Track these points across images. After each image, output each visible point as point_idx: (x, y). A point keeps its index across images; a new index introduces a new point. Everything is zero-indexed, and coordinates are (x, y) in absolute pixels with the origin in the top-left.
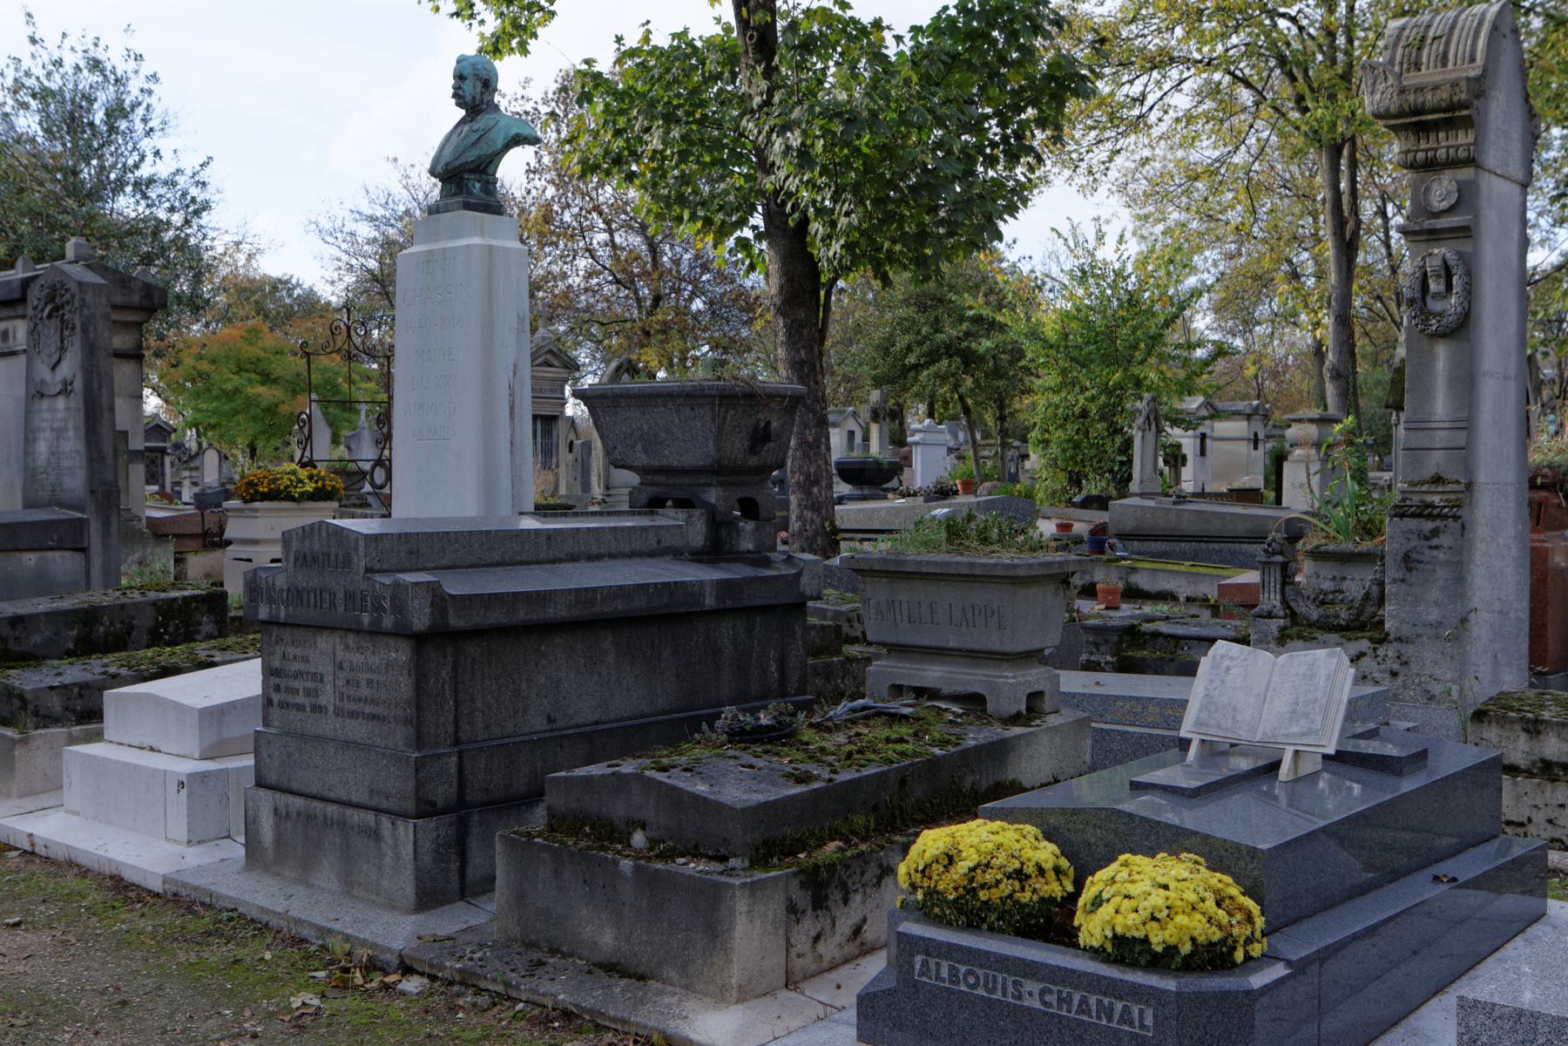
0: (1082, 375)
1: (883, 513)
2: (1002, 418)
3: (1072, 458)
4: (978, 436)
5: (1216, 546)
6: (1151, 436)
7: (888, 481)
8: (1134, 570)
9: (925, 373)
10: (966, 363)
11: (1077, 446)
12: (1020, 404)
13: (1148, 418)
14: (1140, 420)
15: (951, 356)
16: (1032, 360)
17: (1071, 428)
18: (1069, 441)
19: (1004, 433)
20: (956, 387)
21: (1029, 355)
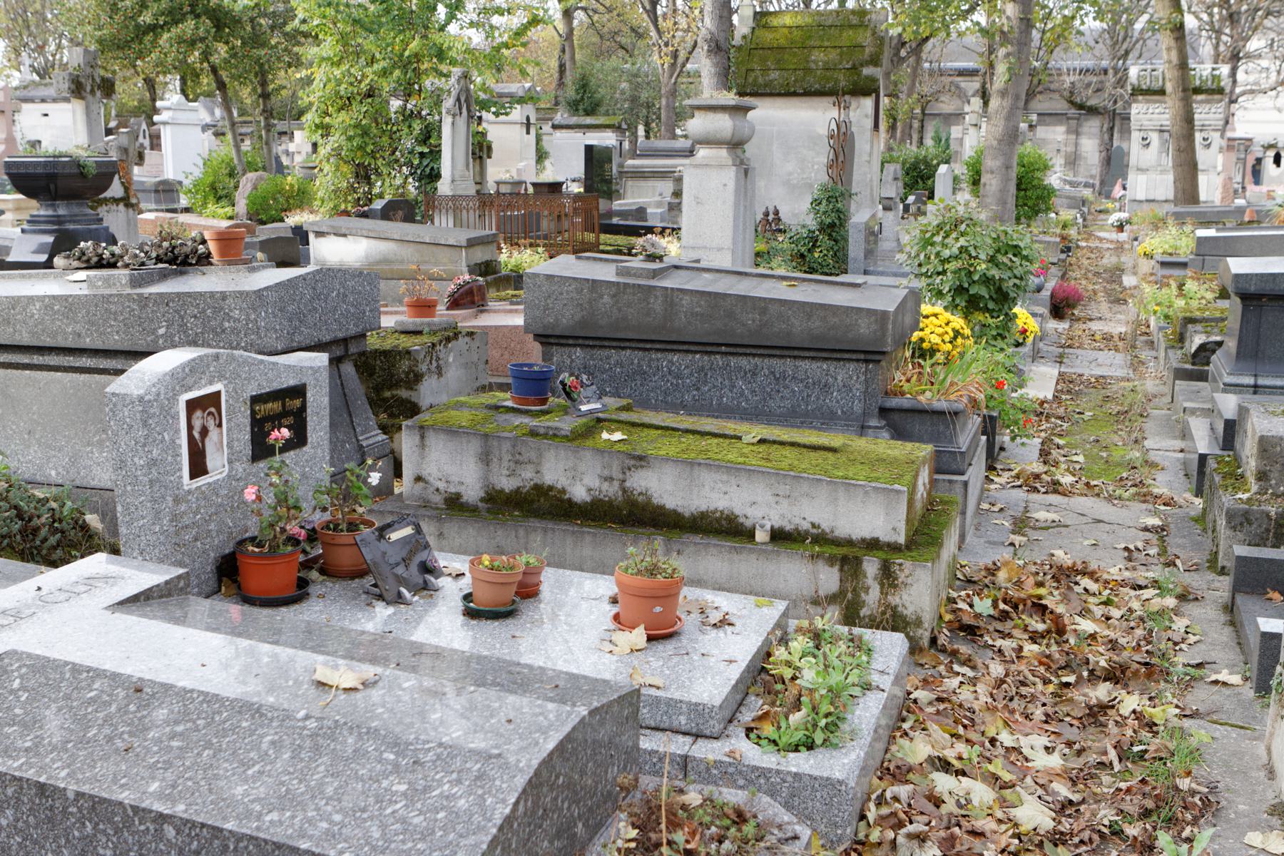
0: (368, 43)
1: (35, 309)
2: (265, 96)
3: (360, 148)
4: (235, 113)
5: (743, 362)
6: (462, 121)
7: (106, 188)
8: (641, 460)
9: (166, 36)
10: (219, 26)
11: (365, 133)
12: (283, 78)
13: (458, 100)
14: (449, 103)
15: (198, 16)
16: (304, 21)
17: (360, 110)
18: (355, 127)
19: (268, 113)
20: (206, 56)
21: (301, 15)
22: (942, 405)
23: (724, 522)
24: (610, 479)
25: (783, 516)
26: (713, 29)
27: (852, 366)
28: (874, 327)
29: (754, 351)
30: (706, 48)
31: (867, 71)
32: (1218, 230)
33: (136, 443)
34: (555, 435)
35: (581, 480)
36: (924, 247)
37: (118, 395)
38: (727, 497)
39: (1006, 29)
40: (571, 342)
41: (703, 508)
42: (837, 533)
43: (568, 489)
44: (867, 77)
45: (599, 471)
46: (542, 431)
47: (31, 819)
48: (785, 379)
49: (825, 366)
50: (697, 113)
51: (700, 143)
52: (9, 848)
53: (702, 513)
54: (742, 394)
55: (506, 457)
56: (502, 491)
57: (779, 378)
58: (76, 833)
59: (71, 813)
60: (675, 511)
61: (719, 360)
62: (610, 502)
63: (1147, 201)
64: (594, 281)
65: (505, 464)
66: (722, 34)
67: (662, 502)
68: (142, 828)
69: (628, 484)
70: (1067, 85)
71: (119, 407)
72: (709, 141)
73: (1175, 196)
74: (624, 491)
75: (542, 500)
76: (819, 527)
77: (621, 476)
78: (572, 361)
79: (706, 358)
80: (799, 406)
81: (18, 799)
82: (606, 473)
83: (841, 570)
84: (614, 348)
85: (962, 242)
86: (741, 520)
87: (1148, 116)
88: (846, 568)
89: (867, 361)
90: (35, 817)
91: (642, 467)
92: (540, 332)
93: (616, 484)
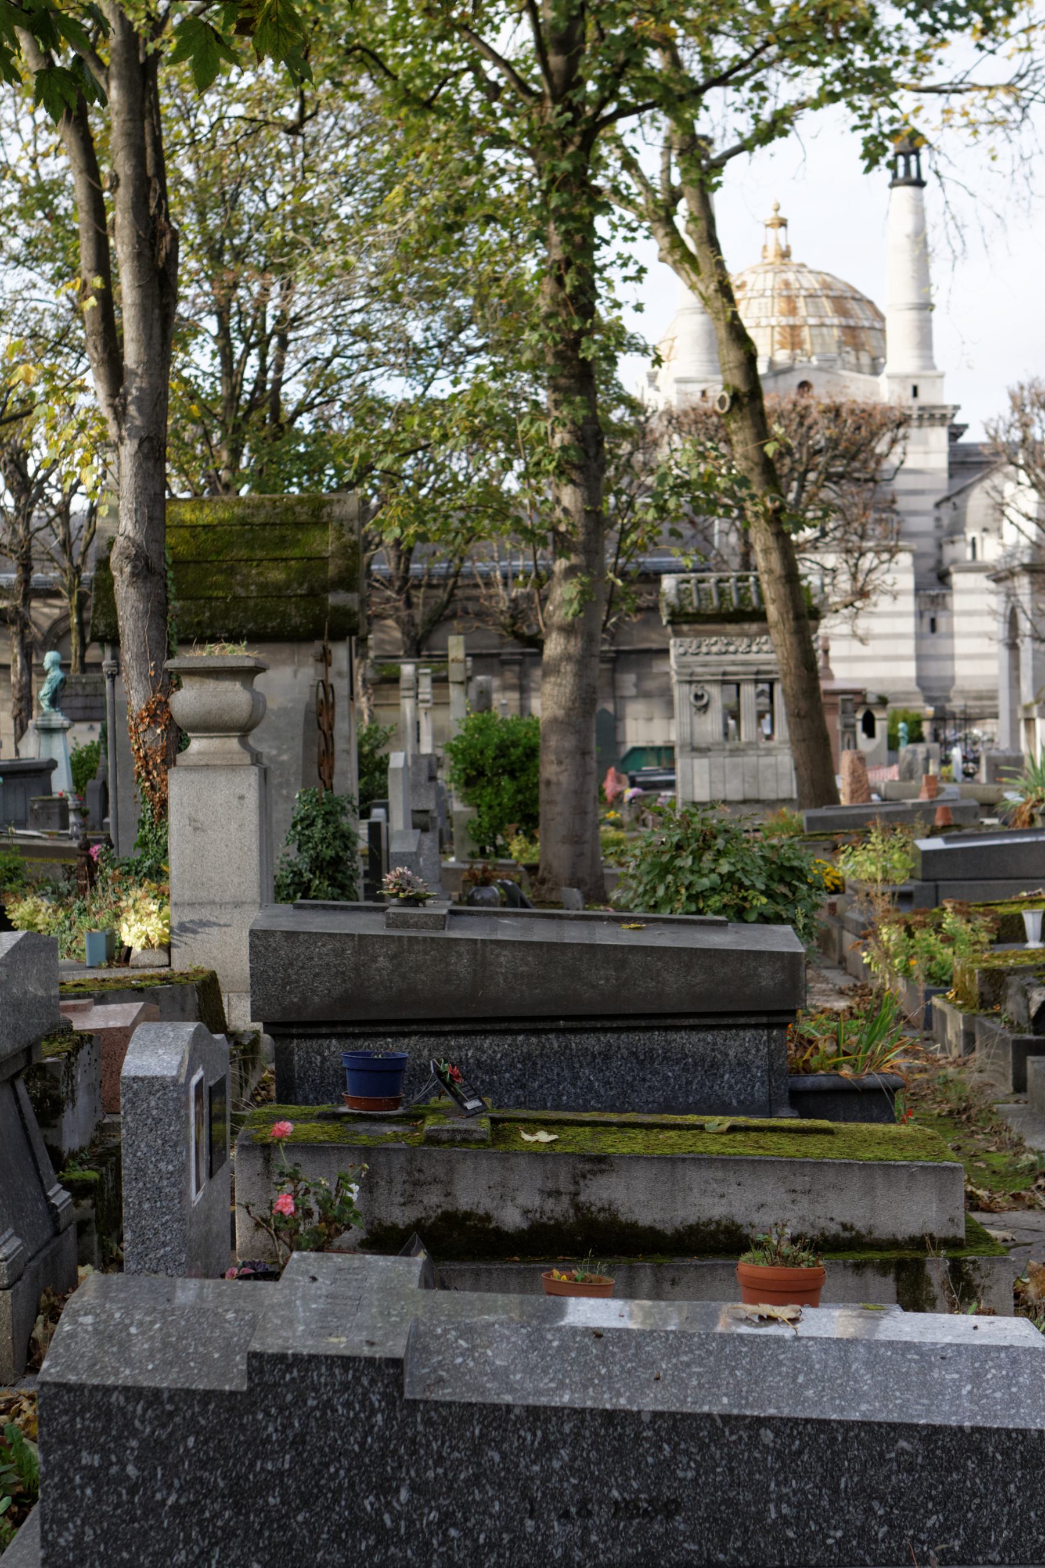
5: (591, 1042)
8: (601, 1162)
22: (878, 1080)
23: (721, 1237)
24: (555, 1194)
25: (802, 1219)
26: (139, 538)
27: (749, 1034)
28: (780, 976)
29: (608, 1024)
30: (128, 570)
31: (333, 599)
32: (947, 840)
33: (165, 1142)
34: (464, 1140)
35: (513, 1199)
36: (662, 878)
37: (142, 1079)
38: (724, 1201)
39: (562, 528)
40: (324, 1030)
41: (692, 1220)
42: (876, 1234)
43: (495, 1214)
44: (336, 609)
45: (539, 1184)
46: (445, 1136)
47: (593, 1455)
48: (652, 1060)
49: (710, 1038)
50: (185, 681)
51: (195, 729)
52: (562, 1494)
53: (690, 1227)
54: (590, 1088)
55: (399, 1178)
56: (394, 1227)
57: (645, 1060)
58: (650, 1460)
59: (646, 1439)
60: (651, 1229)
61: (554, 1042)
62: (558, 1225)
63: (745, 802)
64: (361, 937)
65: (398, 1187)
66: (154, 546)
67: (631, 1218)
68: (734, 1438)
69: (582, 1198)
70: (504, 605)
71: (142, 1096)
72: (212, 726)
73: (800, 792)
74: (577, 1207)
75: (455, 1234)
76: (852, 1228)
77: (572, 1188)
78: (324, 1059)
79: (534, 1040)
80: (676, 1098)
81: (578, 1434)
82: (550, 1185)
83: (897, 1279)
84: (391, 1035)
85: (725, 867)
86: (746, 1231)
87: (701, 658)
88: (903, 1275)
89: (769, 1026)
90: (598, 1451)
91: (602, 1171)
92: (277, 1017)
93: (565, 1200)
